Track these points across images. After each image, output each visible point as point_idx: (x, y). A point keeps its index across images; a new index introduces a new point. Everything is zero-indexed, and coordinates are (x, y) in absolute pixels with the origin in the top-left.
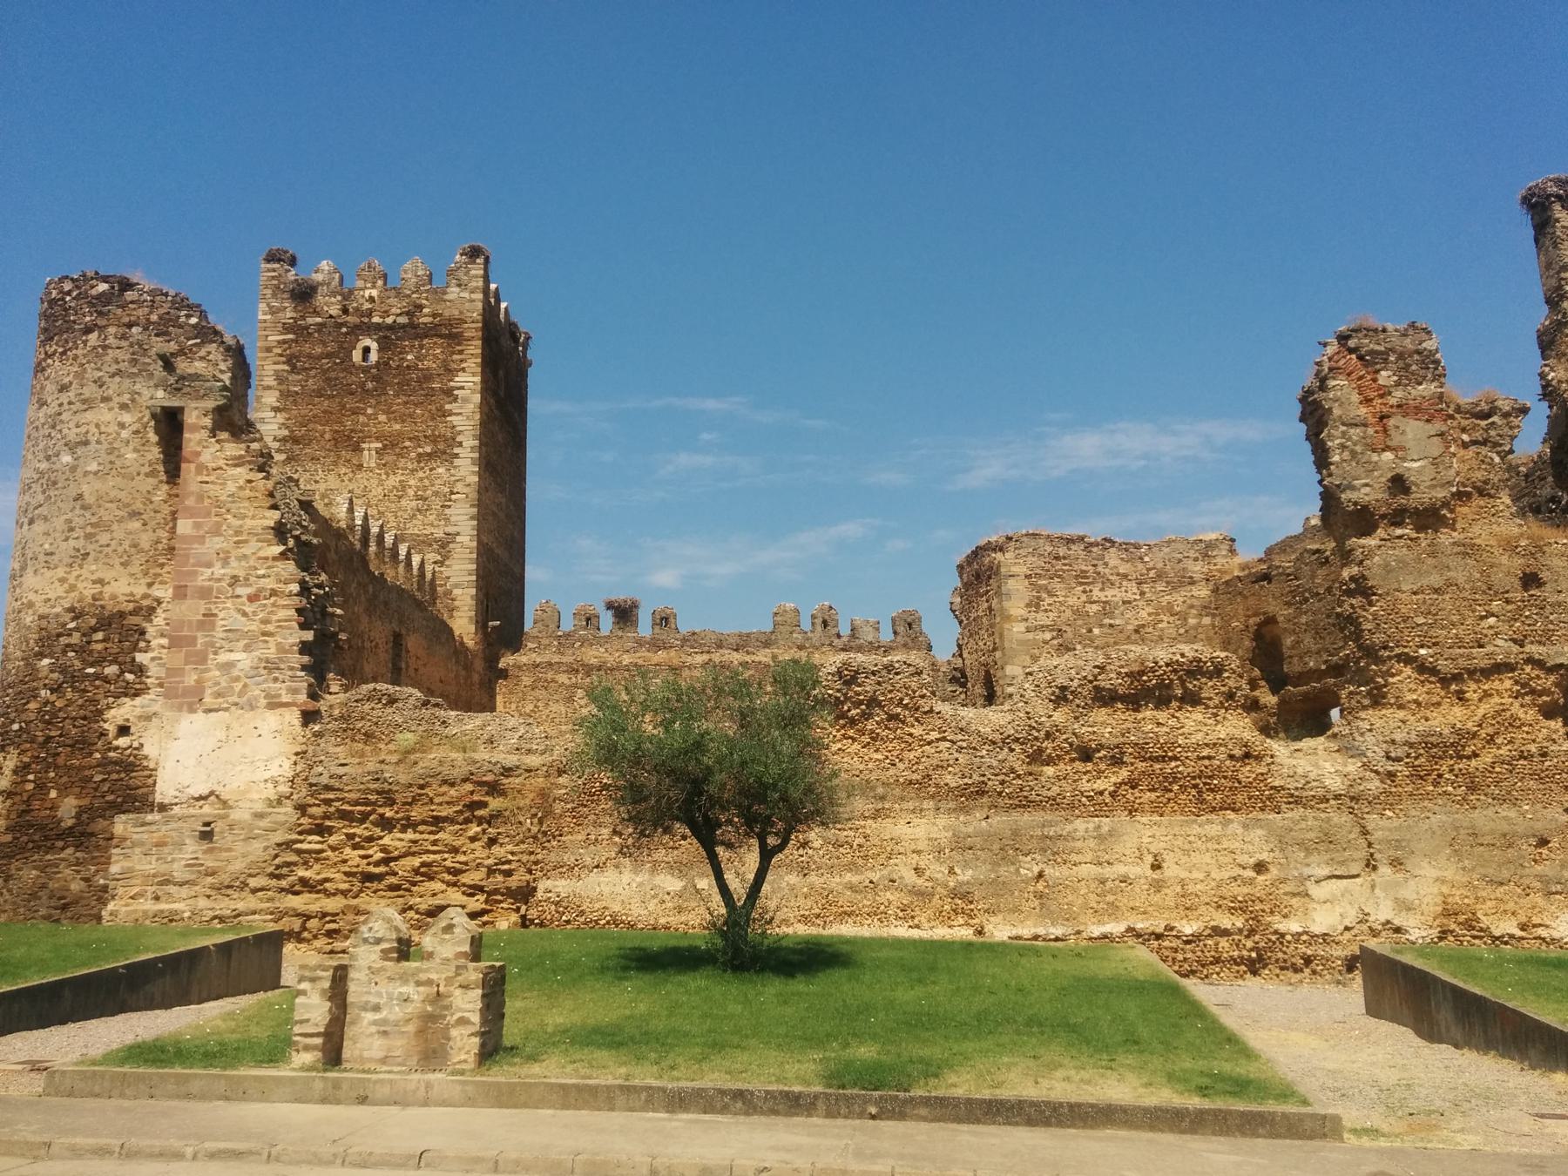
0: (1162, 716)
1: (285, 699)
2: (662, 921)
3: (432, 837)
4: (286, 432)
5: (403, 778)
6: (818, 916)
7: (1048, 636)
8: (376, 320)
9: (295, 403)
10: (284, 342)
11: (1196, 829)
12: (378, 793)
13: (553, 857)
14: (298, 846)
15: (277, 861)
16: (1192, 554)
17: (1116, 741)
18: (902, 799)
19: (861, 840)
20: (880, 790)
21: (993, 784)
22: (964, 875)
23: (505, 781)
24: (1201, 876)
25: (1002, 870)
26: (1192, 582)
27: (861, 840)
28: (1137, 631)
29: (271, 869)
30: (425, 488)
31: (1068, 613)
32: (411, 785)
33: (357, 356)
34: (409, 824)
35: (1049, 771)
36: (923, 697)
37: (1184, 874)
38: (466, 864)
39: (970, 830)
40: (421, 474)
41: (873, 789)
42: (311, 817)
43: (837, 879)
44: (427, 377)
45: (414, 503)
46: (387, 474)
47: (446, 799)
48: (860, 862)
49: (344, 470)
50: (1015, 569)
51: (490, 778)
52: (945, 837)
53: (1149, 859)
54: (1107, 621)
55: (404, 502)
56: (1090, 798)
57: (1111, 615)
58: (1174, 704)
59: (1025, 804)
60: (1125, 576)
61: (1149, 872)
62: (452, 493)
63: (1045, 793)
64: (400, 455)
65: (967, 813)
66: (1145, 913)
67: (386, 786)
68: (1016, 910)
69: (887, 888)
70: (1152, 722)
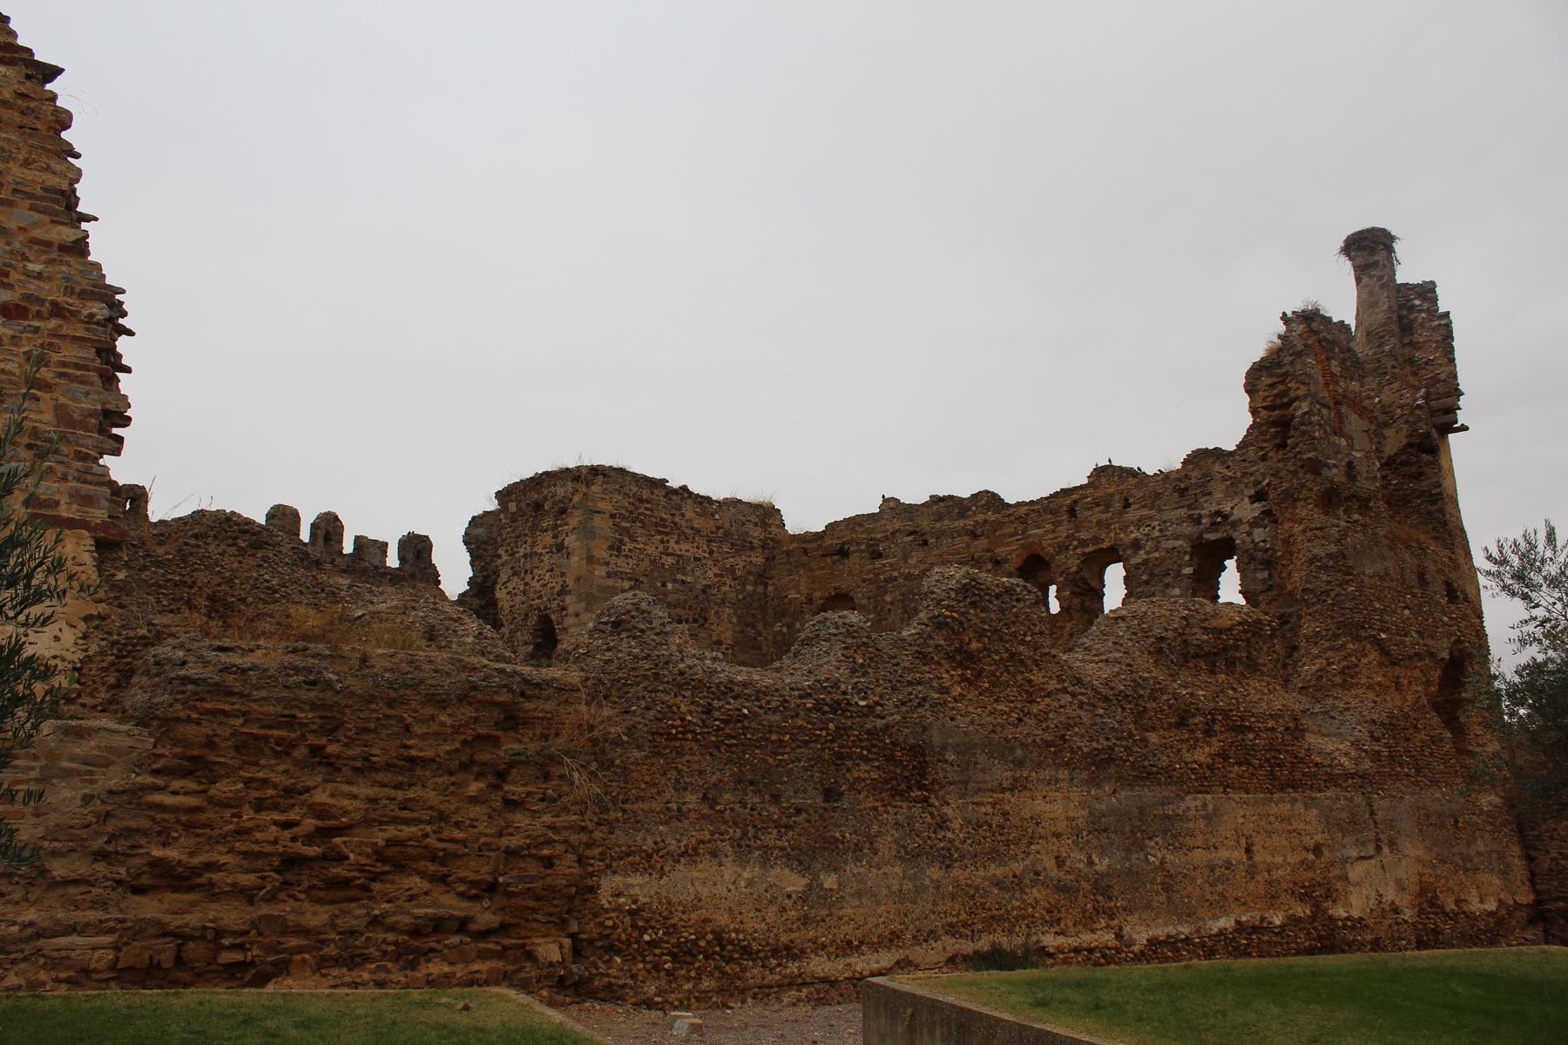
1: (65, 511)
2: (784, 939)
3: (400, 795)
6: (965, 925)
7: (626, 585)
11: (1273, 809)
12: (313, 706)
13: (621, 837)
14: (157, 798)
15: (111, 826)
16: (754, 519)
18: (1039, 765)
19: (998, 819)
21: (1119, 751)
22: (1102, 865)
23: (529, 705)
26: (752, 548)
28: (704, 591)
29: (99, 843)
31: (647, 561)
32: (371, 699)
34: (366, 768)
37: (1269, 859)
38: (464, 842)
42: (177, 742)
43: (982, 873)
47: (434, 727)
48: (1002, 849)
50: (602, 506)
51: (504, 697)
54: (679, 576)
57: (683, 571)
60: (698, 531)
65: (1098, 786)
67: (329, 697)
68: (1148, 906)
69: (1034, 883)
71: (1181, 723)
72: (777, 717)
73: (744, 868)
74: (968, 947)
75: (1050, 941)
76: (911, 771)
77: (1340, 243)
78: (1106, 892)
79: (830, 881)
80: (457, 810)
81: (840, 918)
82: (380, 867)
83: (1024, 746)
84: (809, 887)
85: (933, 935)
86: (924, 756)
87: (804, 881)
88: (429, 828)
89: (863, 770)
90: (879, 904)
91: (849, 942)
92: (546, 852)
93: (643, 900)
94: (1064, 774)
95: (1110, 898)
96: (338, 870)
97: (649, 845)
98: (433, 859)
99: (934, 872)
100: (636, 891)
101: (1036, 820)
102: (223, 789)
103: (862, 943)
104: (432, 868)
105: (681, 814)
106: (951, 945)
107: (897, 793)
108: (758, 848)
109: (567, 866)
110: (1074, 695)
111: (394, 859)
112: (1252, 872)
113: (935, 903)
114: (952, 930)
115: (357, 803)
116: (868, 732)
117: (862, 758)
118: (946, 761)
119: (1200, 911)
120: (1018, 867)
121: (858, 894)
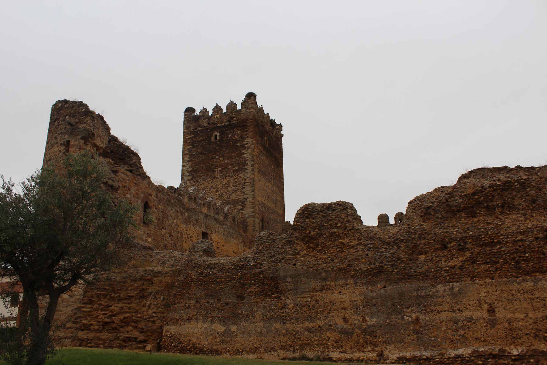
0: (490, 219)
2: (215, 347)
3: (129, 306)
4: (191, 169)
5: (118, 279)
6: (290, 346)
8: (219, 125)
9: (194, 158)
10: (191, 138)
11: (516, 286)
12: (109, 286)
13: (171, 315)
14: (83, 309)
17: (460, 236)
18: (336, 279)
19: (314, 303)
20: (324, 275)
21: (388, 267)
22: (371, 321)
24: (522, 316)
25: (393, 317)
27: (314, 303)
29: (73, 320)
30: (236, 182)
32: (120, 282)
33: (213, 138)
34: (120, 300)
35: (422, 257)
36: (348, 221)
37: (509, 316)
38: (140, 317)
39: (374, 294)
40: (234, 177)
41: (320, 274)
44: (236, 141)
45: (232, 188)
46: (223, 179)
47: (133, 287)
49: (209, 179)
52: (359, 299)
53: (486, 307)
55: (229, 188)
56: (447, 271)
58: (497, 211)
59: (409, 277)
61: (486, 316)
62: (245, 183)
63: (419, 270)
64: (227, 171)
66: (484, 341)
68: (402, 341)
69: (328, 330)
70: (483, 224)
71: (445, 247)
72: (220, 273)
73: (205, 324)
74: (290, 355)
75: (335, 355)
76: (272, 287)
77: (72, 95)
78: (372, 334)
79: (234, 328)
80: (140, 309)
81: (235, 341)
82: (123, 324)
83: (326, 271)
84: (225, 330)
85: (273, 349)
86: (277, 281)
87: (224, 328)
88: (133, 314)
89: (254, 289)
90: (250, 336)
91: (238, 350)
92: (152, 319)
93: (173, 333)
94: (351, 281)
95: (375, 337)
96: (114, 325)
97: (177, 317)
98: (135, 322)
99: (278, 325)
100: (172, 330)
101: (333, 303)
102: (95, 306)
103: (243, 350)
104: (133, 324)
105: (189, 307)
106: (282, 353)
107: (266, 295)
108: (210, 317)
109: (158, 323)
110: (365, 245)
111: (125, 322)
112: (492, 323)
113: (274, 337)
114: (283, 348)
115: (118, 308)
116: (253, 274)
117: (253, 284)
118: (287, 282)
119: (444, 344)
120: (321, 323)
121: (243, 333)
